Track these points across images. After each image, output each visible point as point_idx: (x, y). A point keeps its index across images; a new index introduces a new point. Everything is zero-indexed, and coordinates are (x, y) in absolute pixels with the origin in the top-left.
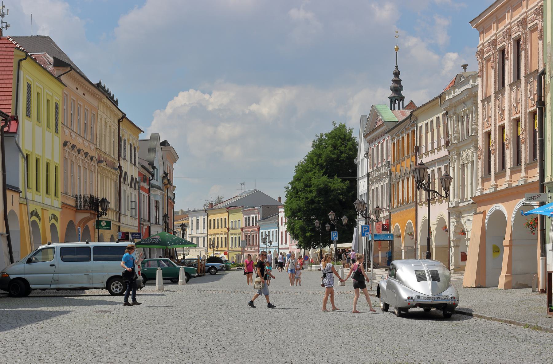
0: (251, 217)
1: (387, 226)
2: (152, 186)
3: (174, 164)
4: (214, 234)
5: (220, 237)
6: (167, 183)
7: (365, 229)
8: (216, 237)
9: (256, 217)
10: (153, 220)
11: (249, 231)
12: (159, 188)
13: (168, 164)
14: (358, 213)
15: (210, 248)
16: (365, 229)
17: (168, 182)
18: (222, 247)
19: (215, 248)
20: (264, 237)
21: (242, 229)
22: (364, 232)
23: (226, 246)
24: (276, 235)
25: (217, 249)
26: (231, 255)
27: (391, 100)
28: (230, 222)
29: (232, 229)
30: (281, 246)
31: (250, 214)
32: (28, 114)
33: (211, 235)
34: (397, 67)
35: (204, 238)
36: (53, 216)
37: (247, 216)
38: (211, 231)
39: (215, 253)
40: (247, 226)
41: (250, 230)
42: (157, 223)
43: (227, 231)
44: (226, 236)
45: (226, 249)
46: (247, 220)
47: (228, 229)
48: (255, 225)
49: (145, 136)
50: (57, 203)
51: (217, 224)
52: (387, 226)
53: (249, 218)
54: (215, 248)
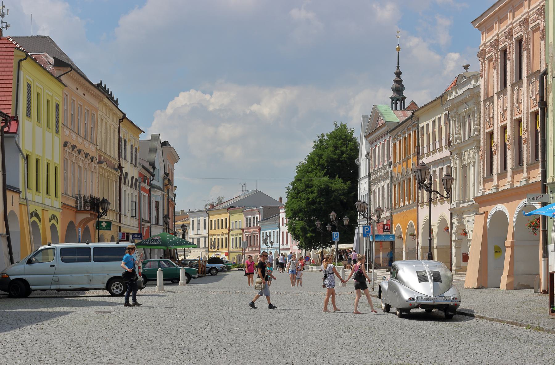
0: (252, 217)
1: (388, 226)
2: (152, 187)
3: (175, 164)
4: (215, 235)
5: (220, 237)
6: (168, 183)
7: (367, 229)
8: (217, 237)
9: (257, 218)
10: (153, 221)
11: (250, 232)
12: (160, 189)
13: (168, 165)
14: (360, 213)
15: (211, 248)
16: (367, 229)
17: (169, 183)
18: (222, 247)
19: (216, 249)
20: (265, 237)
21: (243, 230)
22: (365, 233)
23: (226, 247)
24: (277, 235)
25: (218, 249)
26: (232, 255)
27: (393, 100)
28: (231, 222)
29: (233, 229)
30: (282, 247)
31: (251, 215)
32: (28, 115)
33: (211, 235)
34: (398, 67)
35: (205, 238)
36: (53, 217)
37: (248, 217)
38: (211, 232)
39: (216, 253)
40: (248, 226)
41: (251, 230)
42: (157, 223)
43: (228, 232)
44: (227, 236)
45: (227, 249)
46: (248, 221)
47: (229, 230)
48: (256, 226)
49: (146, 136)
50: (57, 204)
51: (218, 225)
52: (388, 226)
53: (250, 218)
54: (216, 249)
